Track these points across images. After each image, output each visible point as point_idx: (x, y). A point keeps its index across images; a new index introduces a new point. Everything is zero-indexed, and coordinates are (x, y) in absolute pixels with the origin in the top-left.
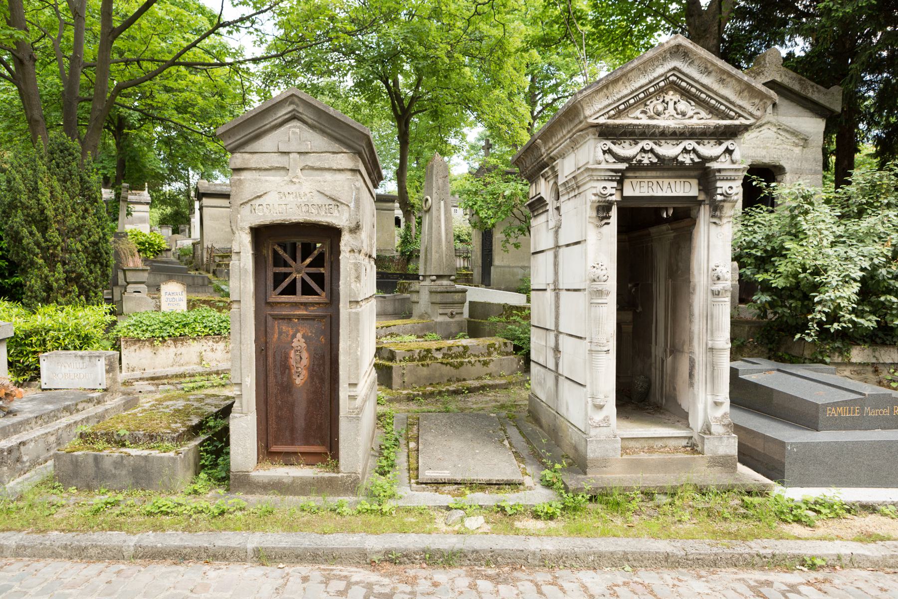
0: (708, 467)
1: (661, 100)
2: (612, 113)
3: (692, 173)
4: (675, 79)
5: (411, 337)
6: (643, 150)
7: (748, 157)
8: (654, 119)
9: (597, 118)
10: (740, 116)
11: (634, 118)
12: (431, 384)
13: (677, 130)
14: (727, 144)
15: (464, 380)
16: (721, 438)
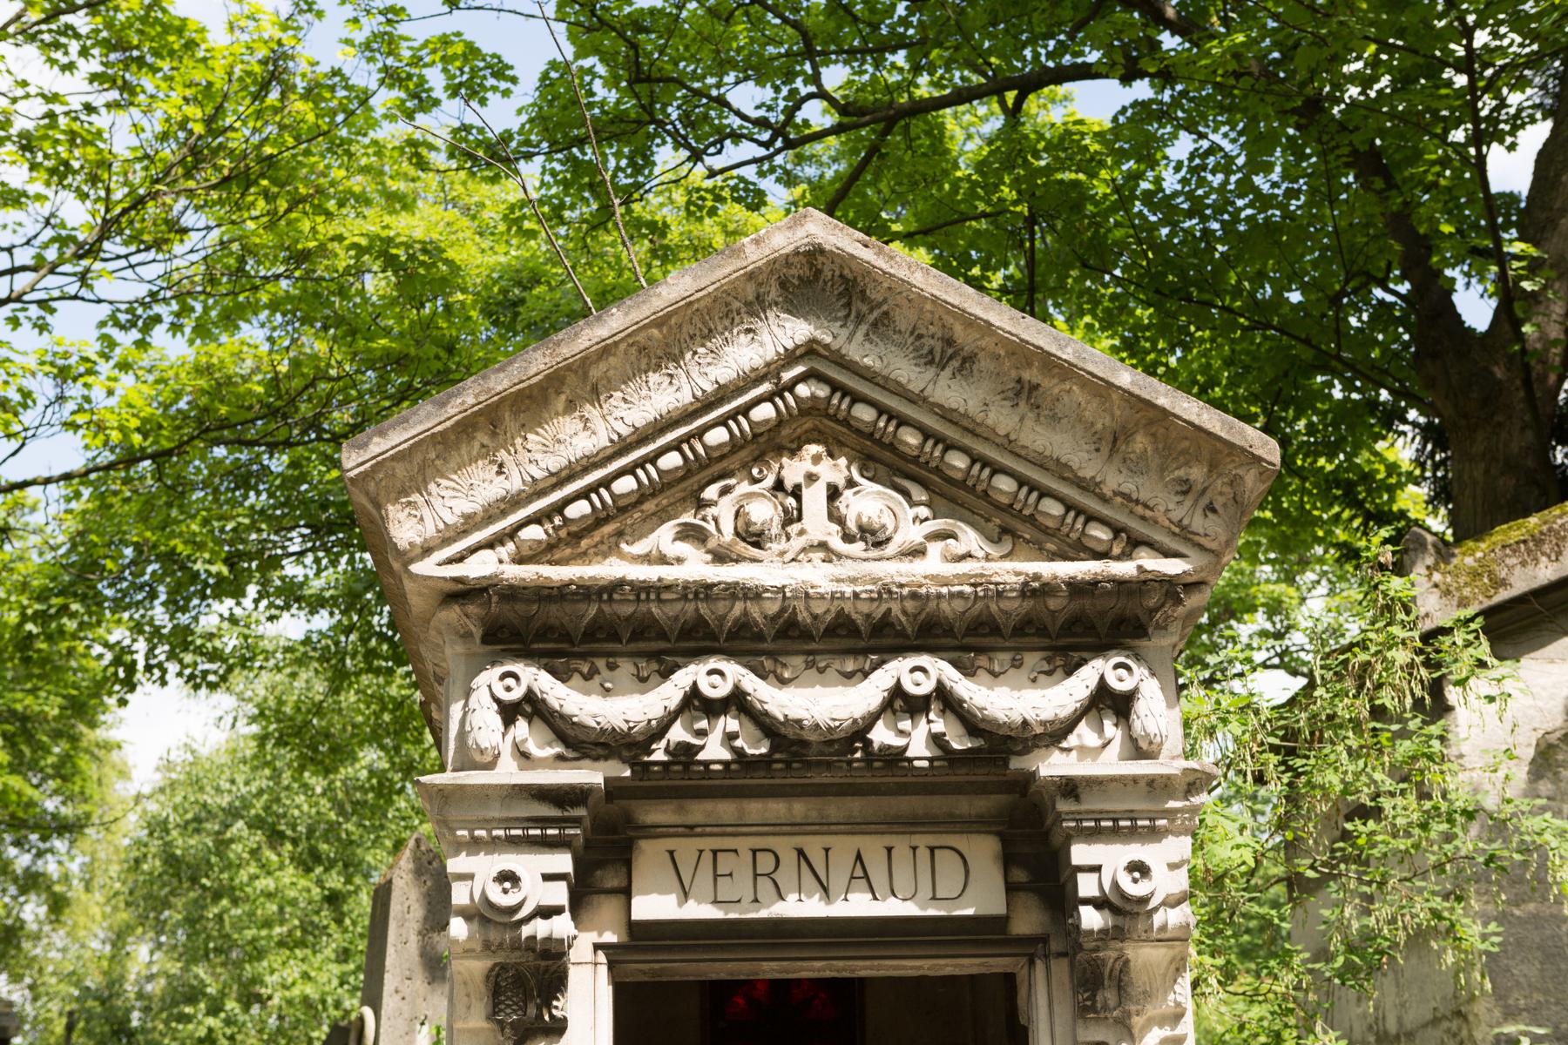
1: (770, 481)
2: (534, 533)
3: (966, 805)
4: (822, 391)
6: (696, 702)
8: (738, 559)
9: (460, 559)
10: (1135, 543)
11: (647, 559)
13: (848, 607)
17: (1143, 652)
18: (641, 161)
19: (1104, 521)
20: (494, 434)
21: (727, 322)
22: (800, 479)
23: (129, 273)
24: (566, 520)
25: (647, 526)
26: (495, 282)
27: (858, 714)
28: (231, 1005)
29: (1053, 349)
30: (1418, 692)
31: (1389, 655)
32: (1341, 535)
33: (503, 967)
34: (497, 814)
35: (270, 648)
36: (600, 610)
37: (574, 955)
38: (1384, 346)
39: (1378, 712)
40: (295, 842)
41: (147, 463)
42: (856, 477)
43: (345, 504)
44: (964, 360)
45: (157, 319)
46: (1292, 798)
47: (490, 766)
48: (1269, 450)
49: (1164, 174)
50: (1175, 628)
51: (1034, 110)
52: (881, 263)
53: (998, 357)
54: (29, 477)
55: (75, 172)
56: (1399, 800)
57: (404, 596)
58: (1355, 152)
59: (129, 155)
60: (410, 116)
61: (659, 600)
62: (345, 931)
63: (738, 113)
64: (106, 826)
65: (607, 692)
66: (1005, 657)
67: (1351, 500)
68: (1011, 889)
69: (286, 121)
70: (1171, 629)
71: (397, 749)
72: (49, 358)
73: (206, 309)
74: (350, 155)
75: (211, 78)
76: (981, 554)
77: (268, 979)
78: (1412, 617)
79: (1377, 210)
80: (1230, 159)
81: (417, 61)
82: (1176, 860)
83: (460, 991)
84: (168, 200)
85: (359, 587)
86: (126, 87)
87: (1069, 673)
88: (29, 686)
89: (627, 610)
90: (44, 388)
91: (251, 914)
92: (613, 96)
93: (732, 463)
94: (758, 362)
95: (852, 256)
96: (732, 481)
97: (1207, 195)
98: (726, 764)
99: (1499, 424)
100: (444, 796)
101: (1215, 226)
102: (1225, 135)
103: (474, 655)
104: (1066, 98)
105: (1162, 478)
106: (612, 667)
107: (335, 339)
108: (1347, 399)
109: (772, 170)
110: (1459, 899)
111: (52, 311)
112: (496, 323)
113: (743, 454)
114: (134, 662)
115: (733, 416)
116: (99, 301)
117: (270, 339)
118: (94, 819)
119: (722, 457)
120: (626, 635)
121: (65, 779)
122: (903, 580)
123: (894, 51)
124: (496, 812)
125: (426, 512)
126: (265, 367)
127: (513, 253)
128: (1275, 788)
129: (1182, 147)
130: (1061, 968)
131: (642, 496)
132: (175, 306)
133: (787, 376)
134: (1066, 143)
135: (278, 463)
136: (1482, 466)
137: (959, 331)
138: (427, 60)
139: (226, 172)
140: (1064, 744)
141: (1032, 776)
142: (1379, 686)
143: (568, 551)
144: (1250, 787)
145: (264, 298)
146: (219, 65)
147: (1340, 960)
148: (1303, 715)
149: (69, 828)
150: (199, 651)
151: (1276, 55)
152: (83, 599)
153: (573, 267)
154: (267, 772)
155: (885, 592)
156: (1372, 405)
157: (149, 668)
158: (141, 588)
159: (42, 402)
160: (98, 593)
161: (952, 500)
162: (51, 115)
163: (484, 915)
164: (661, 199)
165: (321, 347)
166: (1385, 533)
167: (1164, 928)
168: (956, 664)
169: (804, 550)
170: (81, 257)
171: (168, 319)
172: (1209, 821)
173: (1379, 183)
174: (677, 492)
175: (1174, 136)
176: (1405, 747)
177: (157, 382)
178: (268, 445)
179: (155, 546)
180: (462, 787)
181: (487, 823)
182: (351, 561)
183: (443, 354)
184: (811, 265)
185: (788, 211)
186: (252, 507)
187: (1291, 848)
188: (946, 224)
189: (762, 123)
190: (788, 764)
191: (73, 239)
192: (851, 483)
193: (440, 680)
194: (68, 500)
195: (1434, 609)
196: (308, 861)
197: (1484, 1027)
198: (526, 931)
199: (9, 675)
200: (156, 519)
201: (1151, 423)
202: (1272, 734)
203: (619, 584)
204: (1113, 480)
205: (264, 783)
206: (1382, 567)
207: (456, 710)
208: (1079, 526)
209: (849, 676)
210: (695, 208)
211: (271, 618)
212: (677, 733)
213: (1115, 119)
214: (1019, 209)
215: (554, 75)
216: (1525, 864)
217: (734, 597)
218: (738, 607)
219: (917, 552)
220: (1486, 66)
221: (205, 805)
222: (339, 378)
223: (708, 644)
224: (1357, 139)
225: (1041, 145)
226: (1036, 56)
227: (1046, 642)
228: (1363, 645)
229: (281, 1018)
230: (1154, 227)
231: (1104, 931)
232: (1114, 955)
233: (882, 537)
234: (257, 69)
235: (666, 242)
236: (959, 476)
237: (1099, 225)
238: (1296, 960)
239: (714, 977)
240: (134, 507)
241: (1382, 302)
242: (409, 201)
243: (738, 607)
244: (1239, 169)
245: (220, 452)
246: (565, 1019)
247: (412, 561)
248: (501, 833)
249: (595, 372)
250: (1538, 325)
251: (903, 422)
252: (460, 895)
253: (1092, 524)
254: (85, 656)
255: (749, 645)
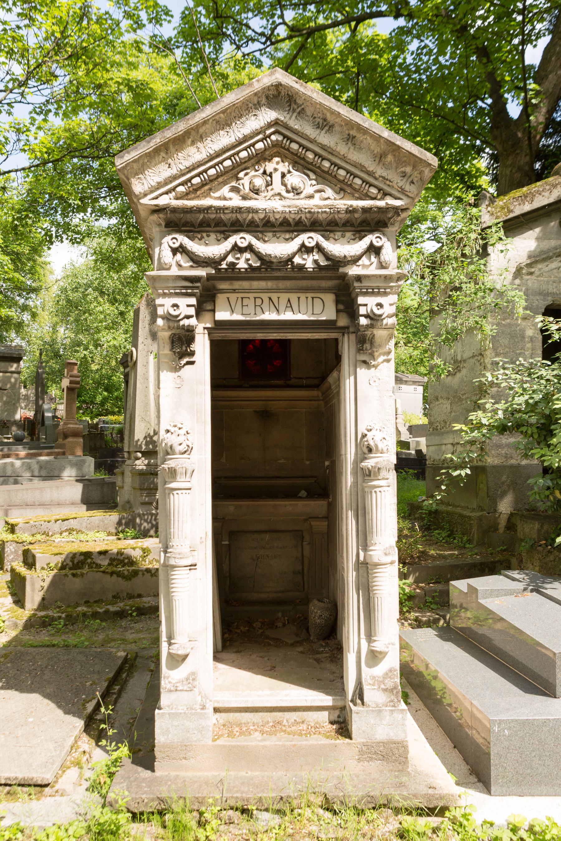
0: (359, 760)
1: (261, 171)
2: (181, 189)
3: (325, 284)
4: (280, 138)
5: (97, 534)
6: (236, 248)
7: (548, 294)
8: (251, 199)
9: (156, 198)
10: (386, 194)
11: (219, 198)
12: (87, 602)
13: (287, 216)
14: (370, 239)
15: (140, 596)
16: (380, 711)
17: (386, 233)
18: (218, 49)
19: (375, 187)
20: (167, 153)
21: (247, 112)
22: (272, 170)
23: (38, 93)
24: (192, 184)
25: (220, 187)
26: (167, 97)
27: (289, 253)
28: (91, 347)
29: (361, 123)
30: (478, 248)
31: (469, 235)
32: (458, 193)
33: (175, 334)
34: (171, 285)
35: (97, 230)
36: (204, 216)
37: (197, 331)
38: (480, 124)
39: (464, 255)
40: (108, 295)
41: (50, 164)
42: (291, 170)
43: (118, 179)
44: (330, 127)
45: (50, 111)
46: (433, 283)
47: (169, 269)
48: (434, 161)
49: (407, 56)
50: (397, 224)
51: (362, 30)
52: (302, 89)
53: (342, 126)
54: (11, 169)
55: (16, 53)
56: (468, 285)
57: (138, 211)
58: (477, 48)
59: (34, 46)
60: (135, 31)
61: (224, 213)
62: (126, 324)
63: (253, 30)
64: (47, 289)
65: (207, 244)
66: (339, 234)
67: (462, 181)
68: (338, 311)
69: (90, 33)
70: (396, 225)
71: (140, 265)
72: (13, 125)
73: (67, 107)
74: (114, 47)
75: (61, 15)
76: (333, 198)
77: (102, 339)
78: (479, 222)
79: (483, 71)
80: (431, 50)
81: (136, 8)
82: (392, 302)
83: (161, 342)
84: (50, 64)
85: (125, 209)
86: (31, 19)
87: (360, 239)
88: (18, 243)
89: (213, 216)
90: (12, 136)
91: (96, 319)
92: (208, 21)
93: (249, 164)
94: (258, 127)
95: (292, 87)
96: (248, 171)
97: (422, 65)
98: (246, 269)
99: (518, 154)
100: (154, 279)
101: (424, 77)
102: (431, 41)
103: (162, 231)
104: (374, 25)
105: (396, 171)
106: (208, 236)
107: (112, 118)
108: (465, 144)
109: (265, 53)
110: (485, 317)
111: (12, 107)
112: (168, 113)
113: (253, 161)
114: (52, 235)
115: (249, 147)
116: (29, 103)
117: (90, 119)
118: (43, 287)
119: (245, 162)
120: (213, 225)
121: (32, 274)
122: (306, 207)
123: (311, 4)
124: (171, 284)
125: (144, 181)
126: (89, 129)
127: (174, 86)
128: (427, 280)
129: (414, 45)
130: (353, 337)
131: (218, 176)
132: (56, 106)
133: (268, 132)
134: (372, 43)
135: (96, 165)
136: (510, 169)
137: (328, 116)
138: (140, 8)
139: (70, 53)
140: (358, 264)
141: (346, 274)
142: (465, 246)
143: (193, 195)
144: (419, 280)
145: (87, 103)
146: (64, 9)
147: (444, 336)
148: (439, 256)
149: (35, 290)
150: (73, 231)
151: (452, 7)
152: (33, 212)
153: (195, 92)
154: (98, 272)
155: (300, 211)
156: (473, 146)
157: (57, 237)
158: (52, 209)
159: (12, 141)
160: (38, 211)
161: (324, 178)
162: (5, 30)
163: (168, 318)
164: (226, 65)
165: (108, 121)
166: (472, 192)
167: (386, 325)
168: (323, 236)
169: (273, 196)
170: (21, 87)
171: (53, 111)
172: (404, 291)
173: (485, 60)
174: (230, 175)
175: (412, 41)
176: (472, 267)
177: (52, 134)
178: (92, 158)
179: (55, 194)
180: (160, 276)
181: (168, 288)
182: (122, 200)
183: (150, 124)
184: (277, 90)
185: (269, 68)
186: (88, 180)
187: (432, 300)
188: (327, 76)
189: (262, 34)
190: (266, 269)
191: (18, 79)
192: (289, 172)
193: (151, 240)
194: (25, 178)
195: (487, 219)
196: (114, 301)
197: (488, 359)
198: (181, 323)
199: (11, 239)
200: (55, 185)
201: (394, 151)
202: (427, 262)
203: (210, 207)
204: (380, 172)
205: (98, 276)
206: (470, 205)
207: (157, 250)
208: (367, 188)
209: (287, 240)
210: (238, 66)
211: (96, 220)
212: (230, 259)
213: (391, 34)
214: (354, 70)
215: (187, 12)
216: (507, 307)
217: (249, 212)
218: (250, 216)
219: (311, 197)
220: (529, 12)
221: (79, 283)
222: (114, 133)
223: (240, 228)
224: (478, 42)
225: (363, 44)
226: (363, 7)
227: (353, 229)
228: (460, 231)
229: (107, 351)
230: (401, 78)
231: (367, 325)
232: (370, 333)
233: (299, 191)
234: (78, 11)
235: (228, 82)
236: (326, 170)
237: (382, 76)
238: (430, 336)
239: (242, 338)
240: (47, 180)
241: (481, 107)
242: (136, 65)
243: (250, 216)
244: (434, 54)
245: (75, 160)
246: (194, 351)
247: (140, 199)
248: (172, 291)
249: (201, 130)
250: (536, 117)
251: (308, 149)
252: (160, 311)
253: (371, 188)
254: (35, 233)
255: (254, 229)
